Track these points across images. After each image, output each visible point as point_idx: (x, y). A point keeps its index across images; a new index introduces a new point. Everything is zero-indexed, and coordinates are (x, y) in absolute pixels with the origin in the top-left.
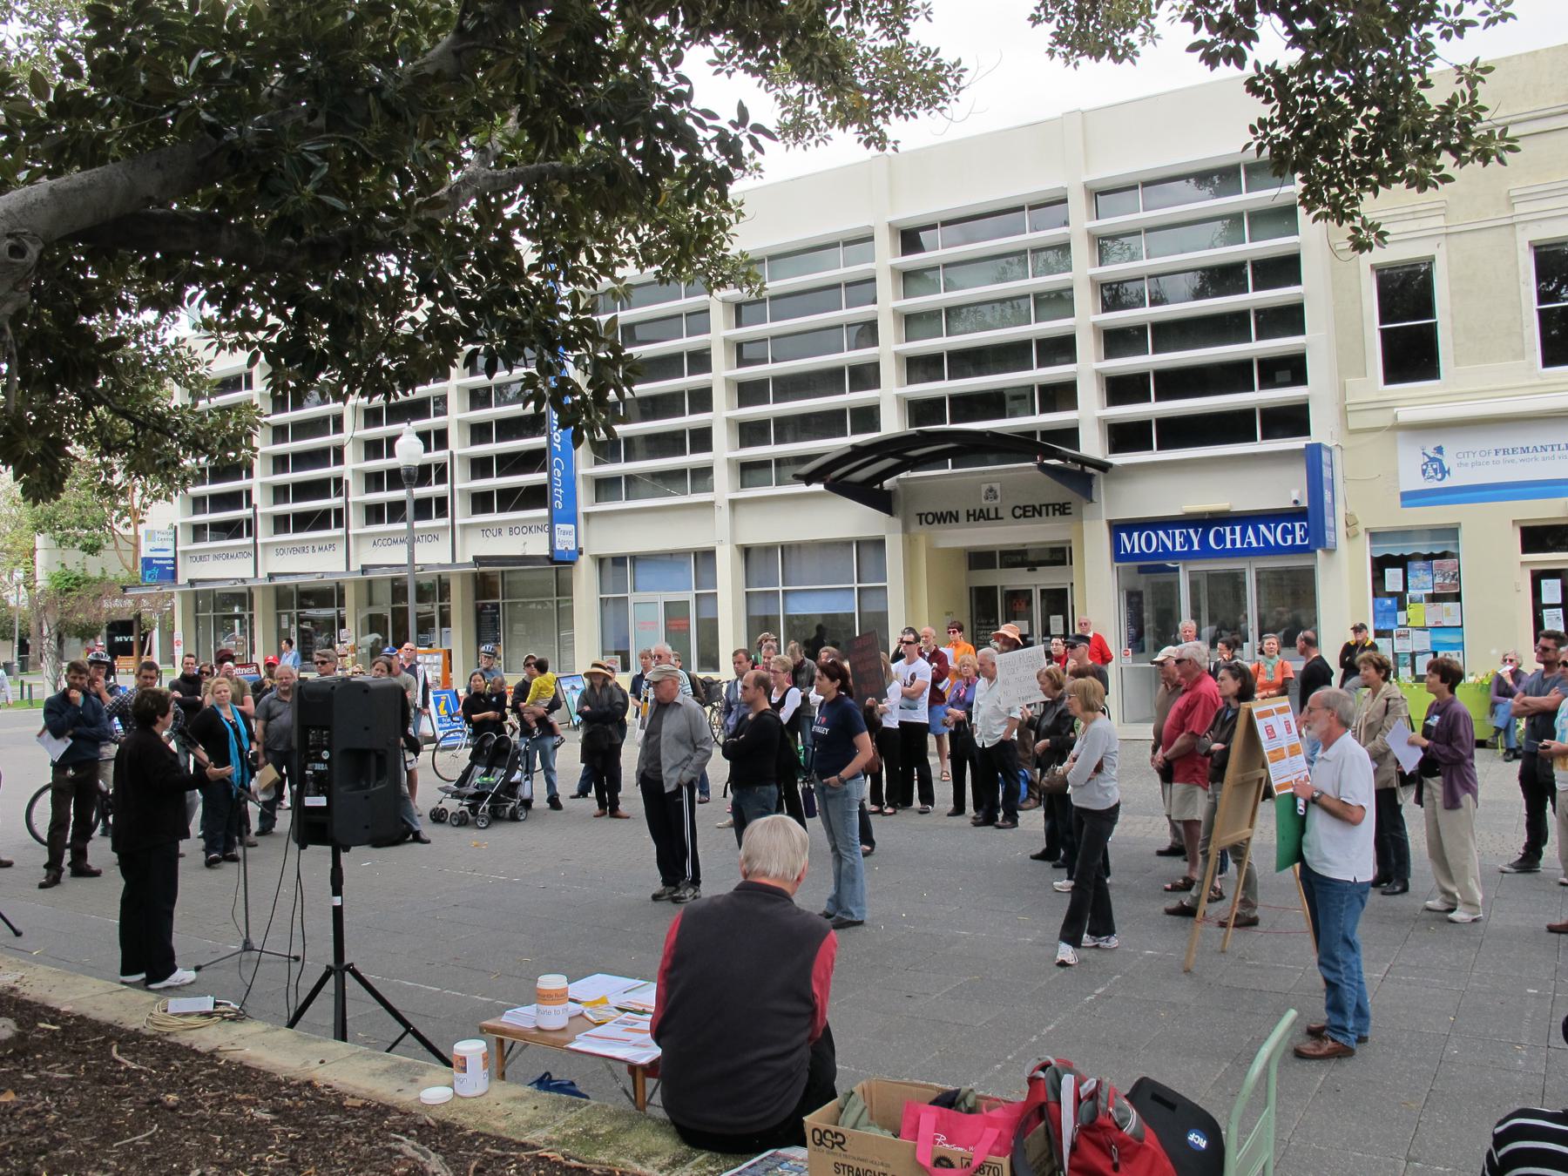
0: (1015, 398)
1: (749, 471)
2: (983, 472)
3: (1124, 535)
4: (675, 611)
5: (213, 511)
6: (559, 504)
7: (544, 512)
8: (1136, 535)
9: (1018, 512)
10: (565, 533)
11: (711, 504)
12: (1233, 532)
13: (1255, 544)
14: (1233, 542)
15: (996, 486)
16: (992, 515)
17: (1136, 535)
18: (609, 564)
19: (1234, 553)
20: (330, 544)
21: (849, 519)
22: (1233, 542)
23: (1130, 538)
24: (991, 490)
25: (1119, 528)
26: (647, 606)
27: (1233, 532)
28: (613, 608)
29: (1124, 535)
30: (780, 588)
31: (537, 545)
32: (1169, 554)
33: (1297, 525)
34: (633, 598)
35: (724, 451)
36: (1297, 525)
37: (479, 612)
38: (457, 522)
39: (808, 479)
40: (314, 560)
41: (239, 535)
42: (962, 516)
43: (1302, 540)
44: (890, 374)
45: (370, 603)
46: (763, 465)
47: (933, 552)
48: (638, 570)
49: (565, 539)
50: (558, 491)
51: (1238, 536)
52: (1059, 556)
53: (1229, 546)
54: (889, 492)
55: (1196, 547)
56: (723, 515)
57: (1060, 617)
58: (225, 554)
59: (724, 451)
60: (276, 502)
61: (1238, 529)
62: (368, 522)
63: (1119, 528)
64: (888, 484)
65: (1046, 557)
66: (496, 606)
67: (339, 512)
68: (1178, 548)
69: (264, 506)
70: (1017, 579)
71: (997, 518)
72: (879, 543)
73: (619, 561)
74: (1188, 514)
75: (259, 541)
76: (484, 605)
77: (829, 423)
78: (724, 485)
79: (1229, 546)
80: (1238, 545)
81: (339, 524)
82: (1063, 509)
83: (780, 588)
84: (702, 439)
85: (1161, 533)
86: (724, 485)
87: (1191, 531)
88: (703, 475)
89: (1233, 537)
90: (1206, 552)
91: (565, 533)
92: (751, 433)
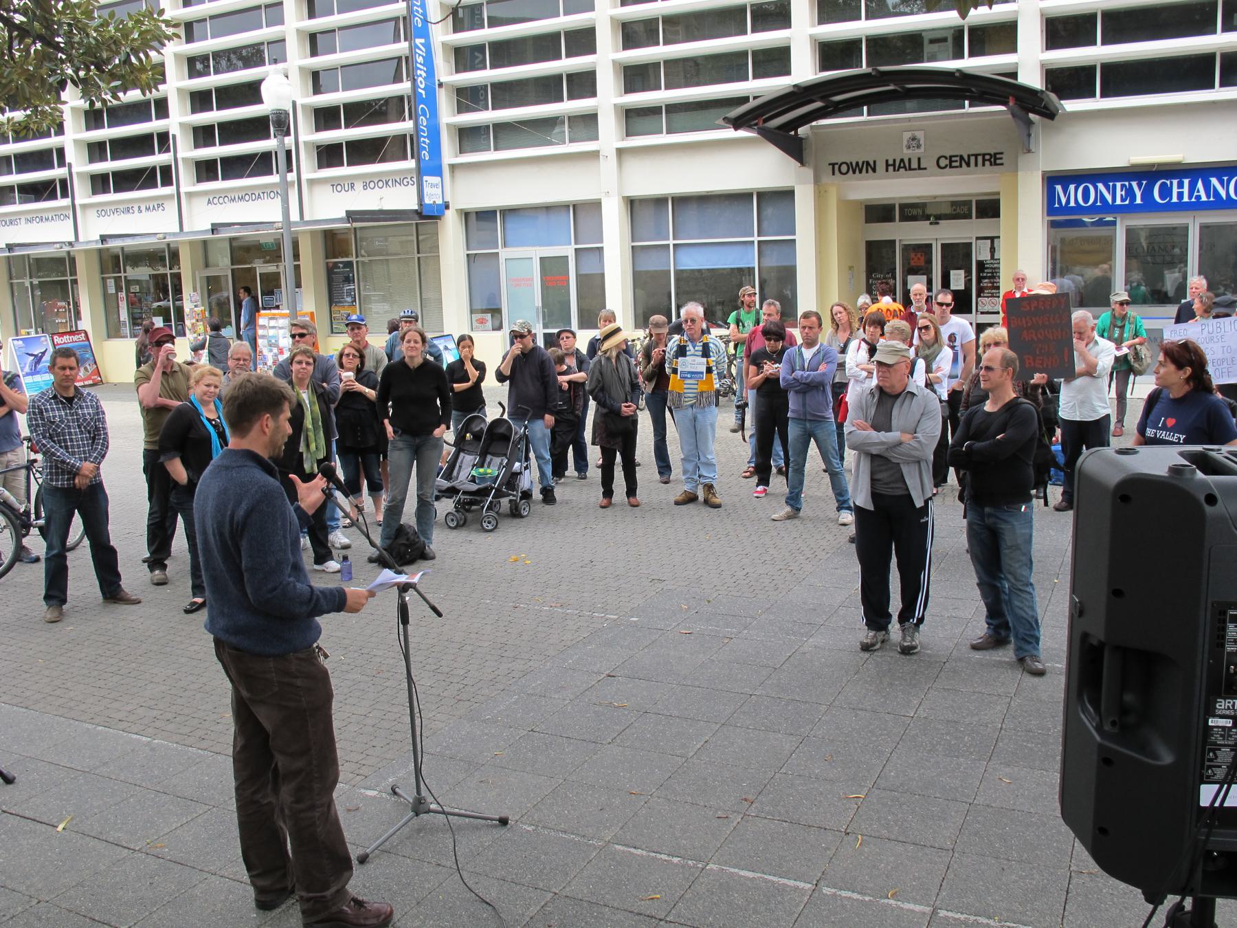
0: (932, 41)
1: (634, 118)
2: (909, 119)
3: (1059, 188)
4: (552, 269)
5: (19, 171)
6: (425, 155)
7: (410, 164)
8: (1072, 187)
9: (943, 162)
10: (433, 186)
11: (595, 155)
12: (1181, 185)
13: (1204, 198)
14: (1180, 195)
15: (920, 135)
16: (914, 165)
17: (1072, 187)
18: (473, 218)
19: (1181, 207)
20: (159, 203)
21: (757, 166)
22: (1180, 195)
23: (1065, 190)
24: (914, 139)
25: (1053, 180)
26: (521, 260)
27: (1181, 185)
28: (480, 265)
29: (1059, 188)
30: (671, 242)
31: (403, 199)
32: (1107, 208)
33: (1118, 185)
34: (504, 253)
35: (609, 97)
36: (1118, 185)
37: (330, 271)
38: (182, 190)
39: (737, 123)
40: (144, 220)
41: (53, 196)
42: (881, 166)
43: (1123, 200)
44: (606, 40)
45: (207, 265)
46: (654, 111)
47: (844, 204)
48: (508, 225)
49: (433, 196)
50: (425, 141)
51: (1186, 190)
52: (989, 208)
53: (1175, 199)
54: (801, 139)
55: (1138, 201)
56: (609, 163)
57: (962, 272)
58: (40, 217)
59: (609, 97)
60: (91, 161)
61: (1186, 182)
62: (95, 192)
63: (1053, 180)
64: (802, 131)
65: (948, 210)
66: (350, 264)
67: (63, 182)
68: (1118, 202)
69: (79, 165)
70: (905, 233)
71: (919, 168)
72: (788, 194)
73: (486, 215)
74: (1133, 166)
75: (77, 202)
76: (336, 265)
77: (730, 66)
78: (610, 133)
79: (1175, 199)
80: (1186, 199)
81: (65, 194)
82: (993, 159)
83: (671, 242)
84: (584, 84)
85: (1101, 186)
86: (610, 133)
87: (1134, 184)
88: (588, 122)
89: (1180, 190)
90: (1149, 205)
91: (433, 186)
92: (636, 77)
